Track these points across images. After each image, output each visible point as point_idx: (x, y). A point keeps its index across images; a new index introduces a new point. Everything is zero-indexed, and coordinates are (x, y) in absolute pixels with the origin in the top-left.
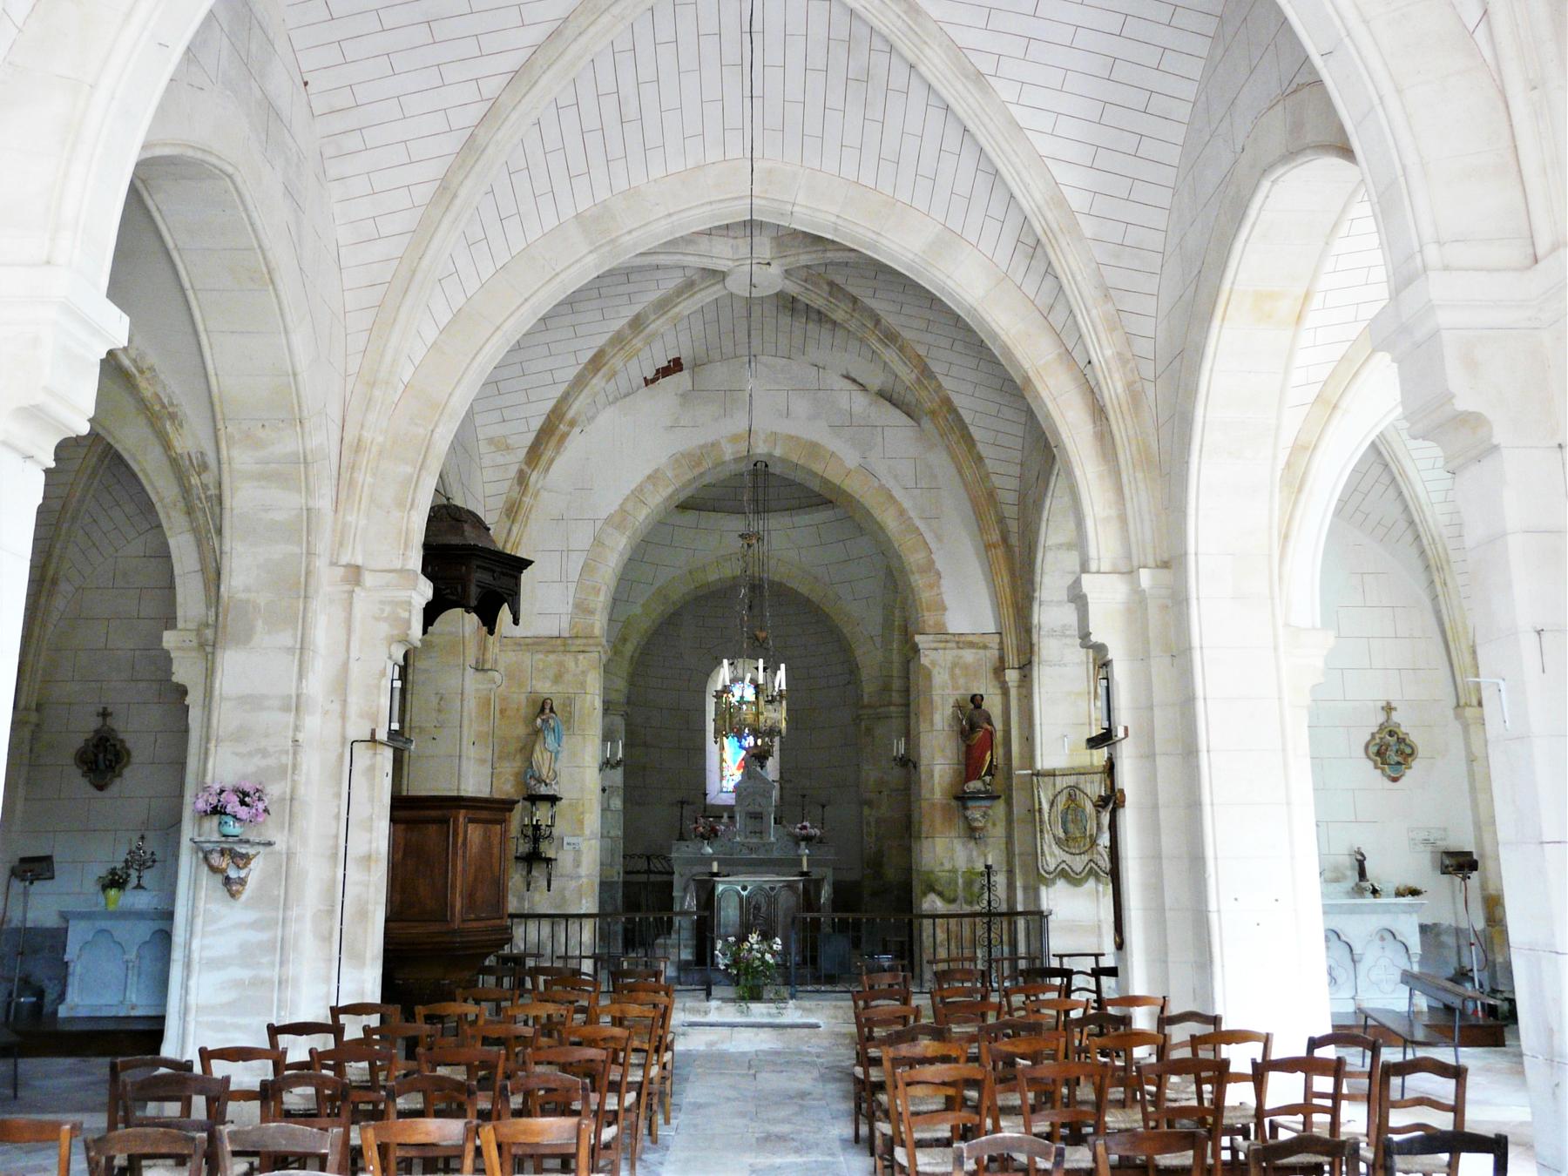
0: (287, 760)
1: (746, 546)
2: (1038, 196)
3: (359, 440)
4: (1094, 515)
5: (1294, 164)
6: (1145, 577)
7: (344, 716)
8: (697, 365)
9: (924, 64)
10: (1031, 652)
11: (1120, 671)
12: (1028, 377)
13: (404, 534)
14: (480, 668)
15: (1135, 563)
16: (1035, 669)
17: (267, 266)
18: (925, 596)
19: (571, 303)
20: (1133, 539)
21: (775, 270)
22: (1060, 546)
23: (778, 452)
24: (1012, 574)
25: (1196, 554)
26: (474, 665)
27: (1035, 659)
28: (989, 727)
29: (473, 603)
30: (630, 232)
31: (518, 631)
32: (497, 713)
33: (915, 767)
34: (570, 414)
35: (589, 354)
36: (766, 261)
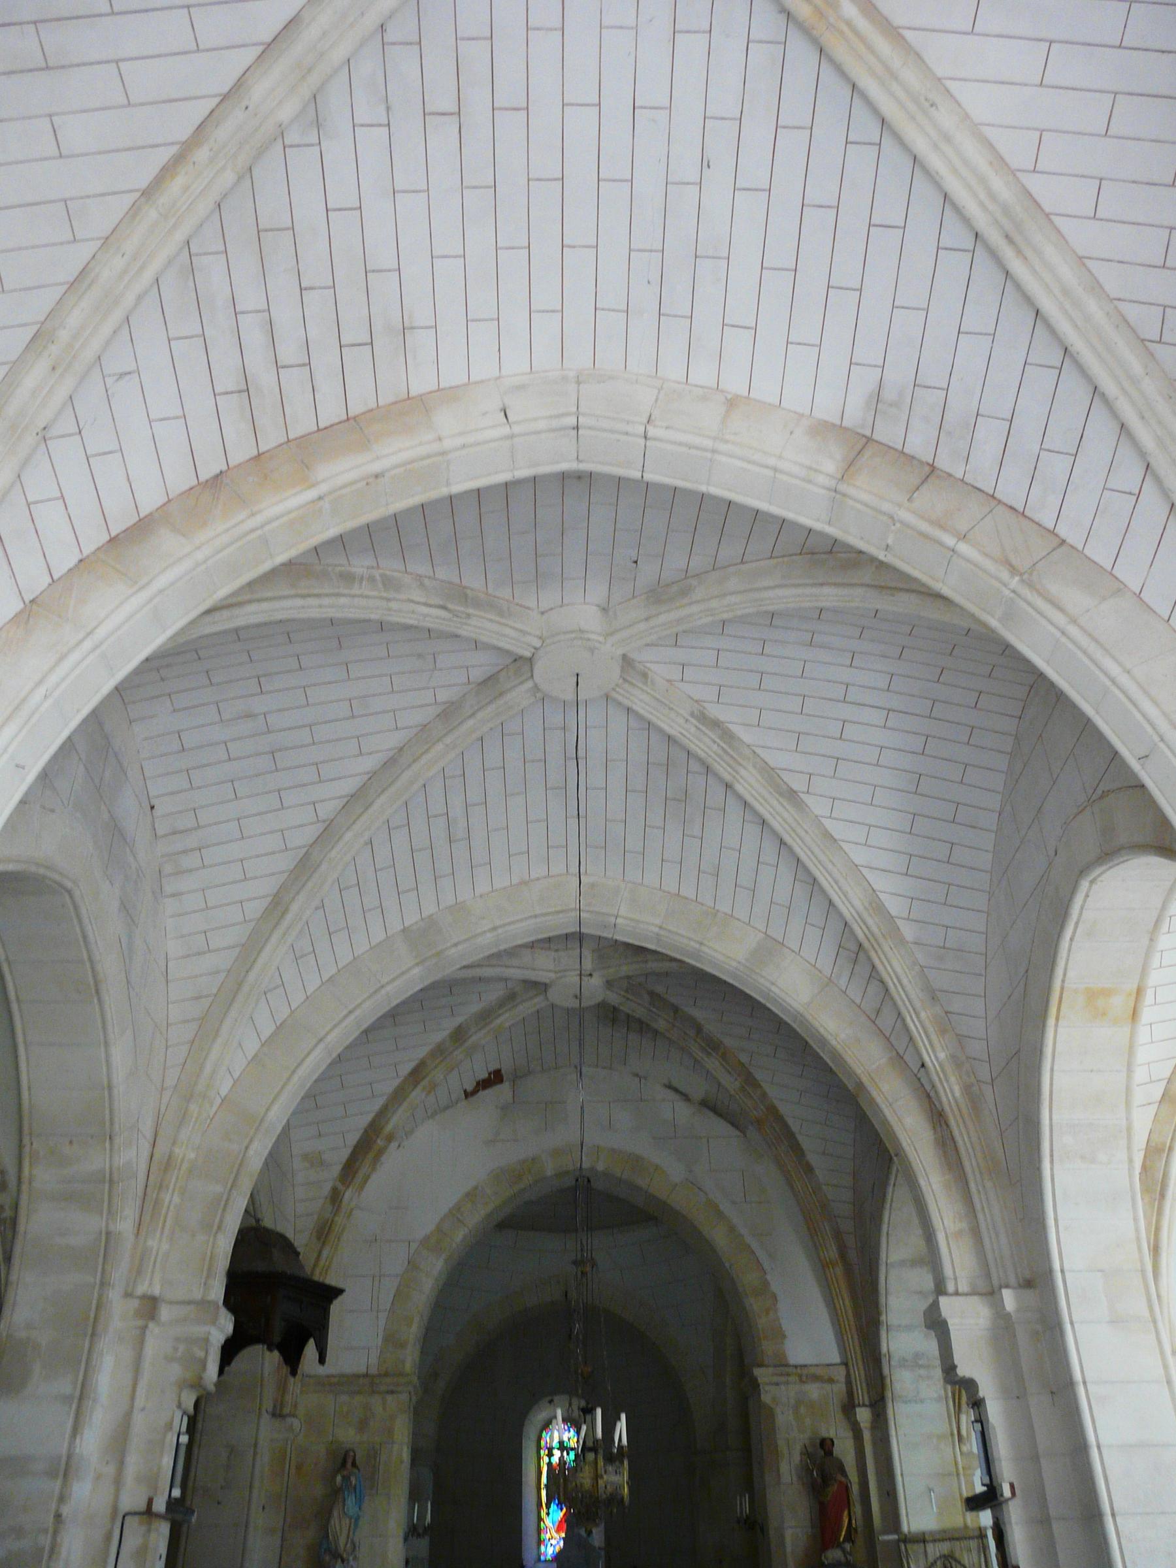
0: (45, 1541)
1: (579, 1273)
2: (857, 903)
3: (170, 1157)
4: (944, 1228)
5: (1111, 864)
6: (1009, 1298)
7: (118, 1482)
8: (516, 1077)
9: (740, 783)
10: (883, 1386)
11: (994, 1410)
12: (861, 1083)
13: (207, 1263)
14: (277, 1414)
15: (995, 1282)
16: (889, 1405)
17: (95, 976)
18: (762, 1322)
19: (393, 1016)
20: (990, 1256)
21: (596, 981)
22: (903, 1263)
23: (600, 1167)
24: (854, 1296)
25: (1062, 1271)
26: (270, 1409)
27: (888, 1394)
28: (843, 1479)
29: (277, 1338)
30: (456, 945)
31: (322, 1370)
32: (293, 1471)
33: (762, 1529)
34: (389, 1128)
35: (412, 1065)
36: (589, 973)
